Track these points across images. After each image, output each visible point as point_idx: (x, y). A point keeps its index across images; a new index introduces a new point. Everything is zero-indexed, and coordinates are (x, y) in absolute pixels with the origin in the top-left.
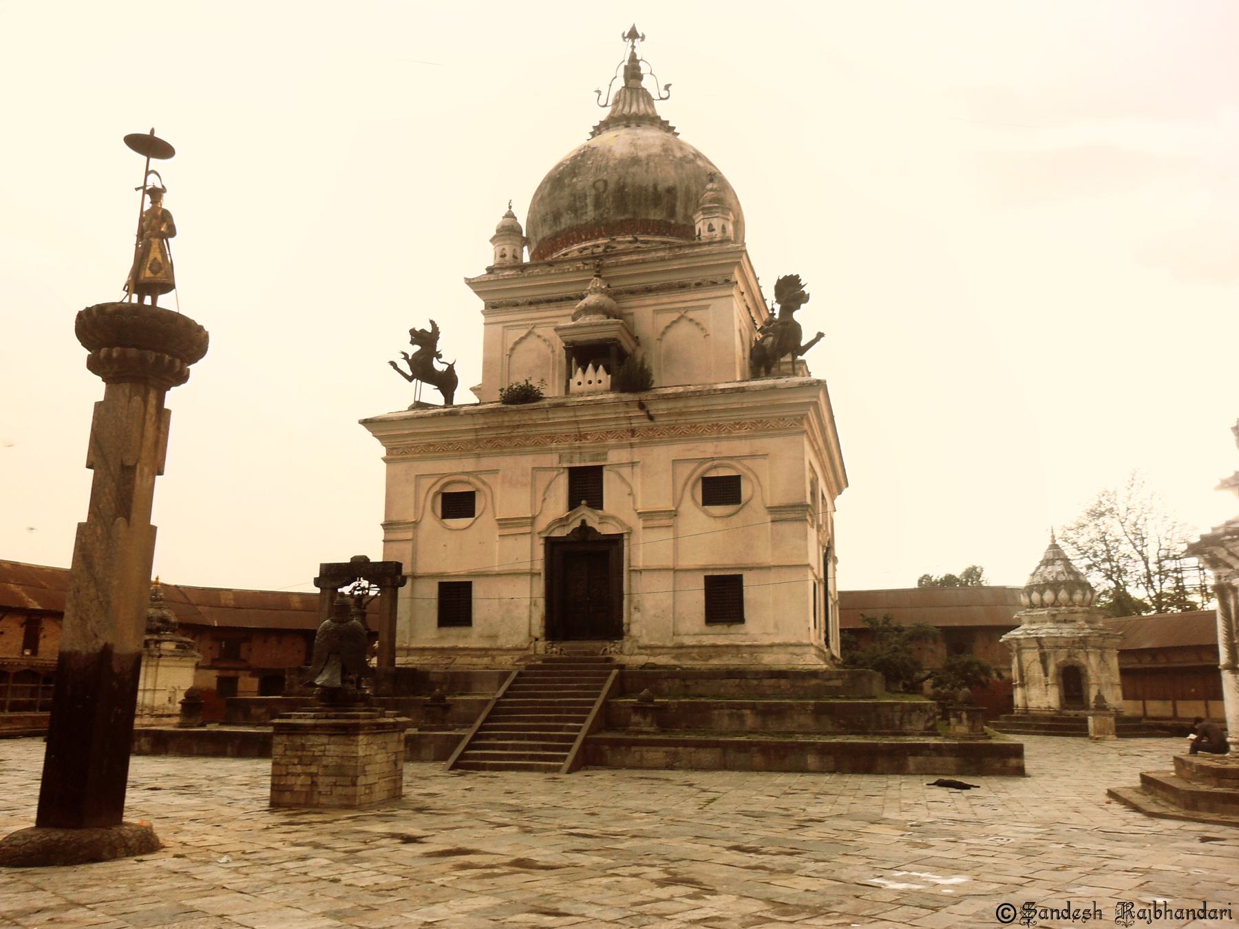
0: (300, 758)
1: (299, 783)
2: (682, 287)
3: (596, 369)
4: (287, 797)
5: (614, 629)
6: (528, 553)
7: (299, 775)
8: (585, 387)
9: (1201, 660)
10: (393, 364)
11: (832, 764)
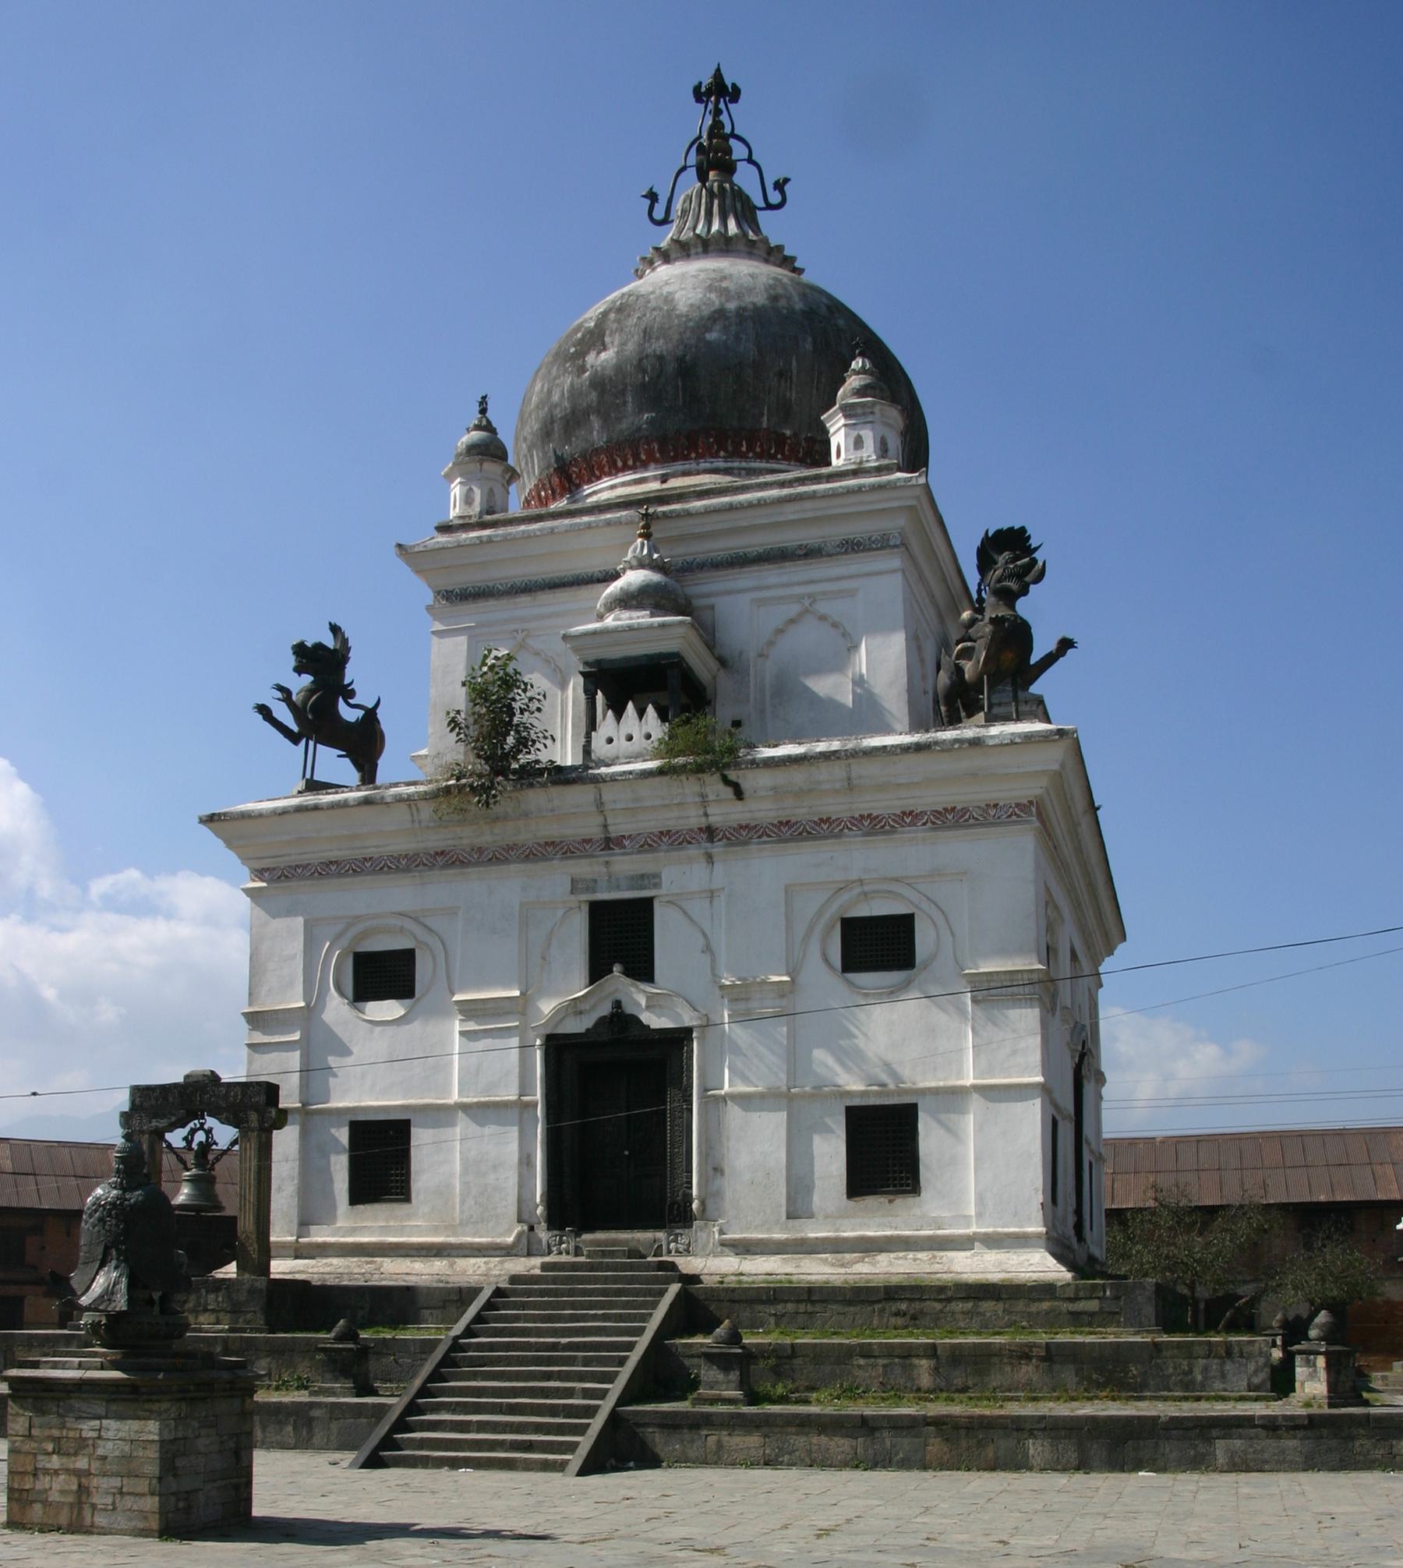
0: (56, 1440)
1: (56, 1486)
2: (810, 553)
3: (641, 713)
4: (37, 1511)
5: (674, 1212)
6: (512, 1070)
7: (56, 1472)
8: (621, 745)
9: (293, 957)
10: (264, 711)
11: (1073, 1456)
